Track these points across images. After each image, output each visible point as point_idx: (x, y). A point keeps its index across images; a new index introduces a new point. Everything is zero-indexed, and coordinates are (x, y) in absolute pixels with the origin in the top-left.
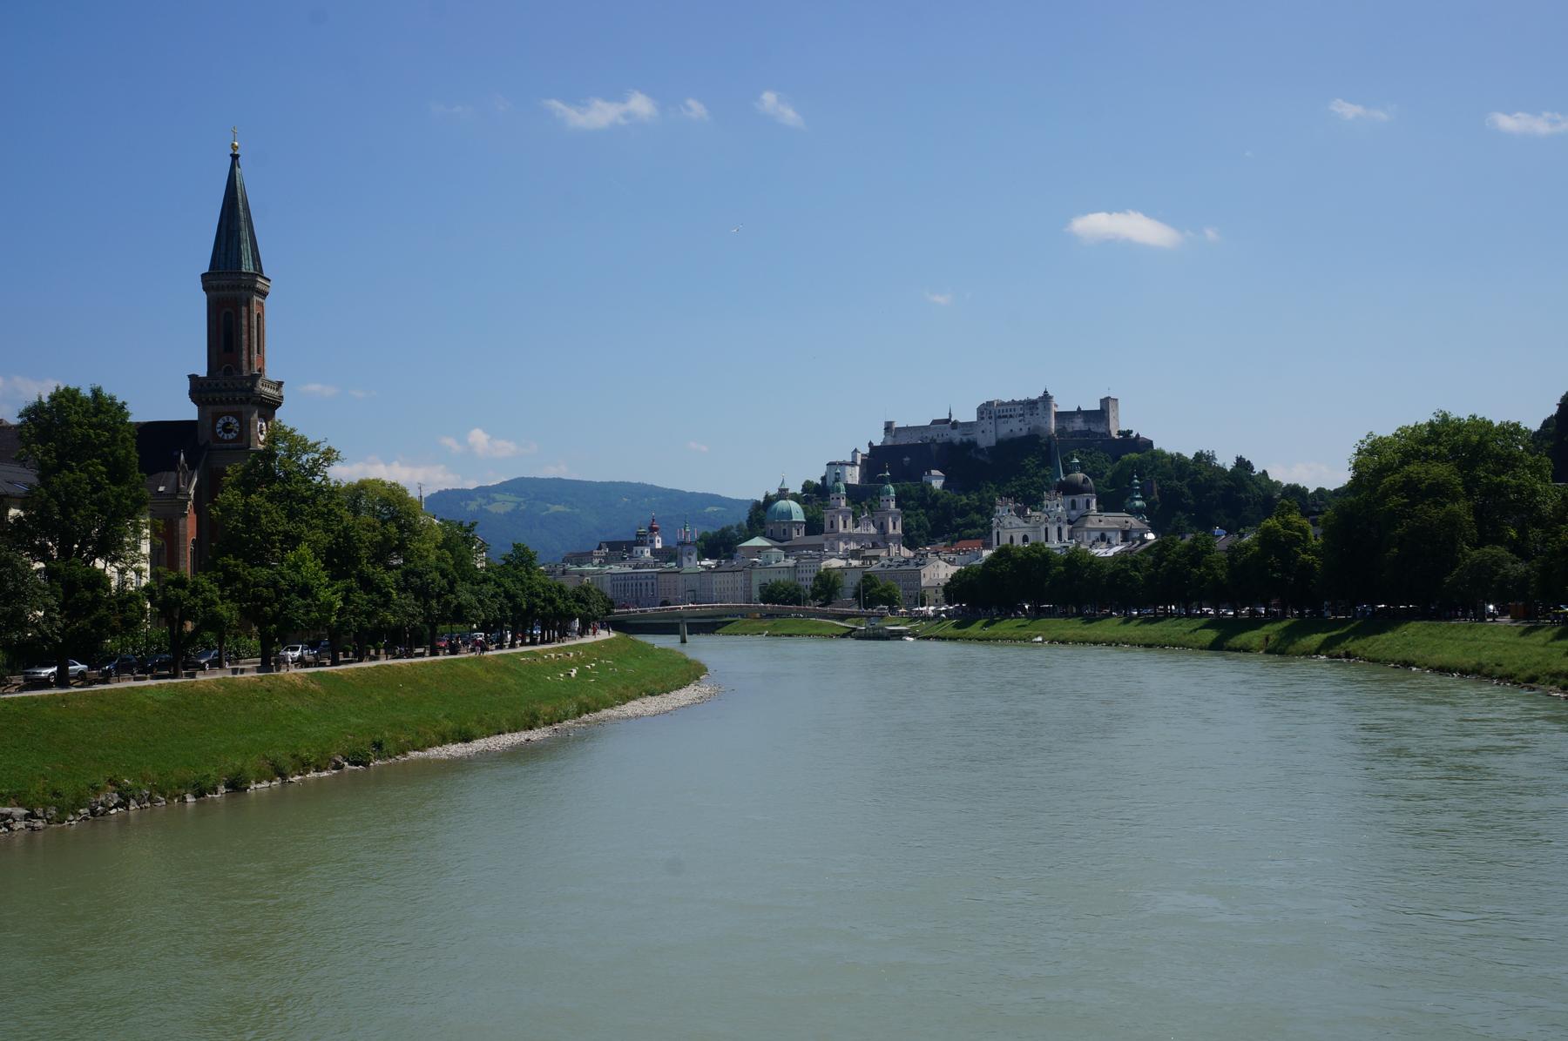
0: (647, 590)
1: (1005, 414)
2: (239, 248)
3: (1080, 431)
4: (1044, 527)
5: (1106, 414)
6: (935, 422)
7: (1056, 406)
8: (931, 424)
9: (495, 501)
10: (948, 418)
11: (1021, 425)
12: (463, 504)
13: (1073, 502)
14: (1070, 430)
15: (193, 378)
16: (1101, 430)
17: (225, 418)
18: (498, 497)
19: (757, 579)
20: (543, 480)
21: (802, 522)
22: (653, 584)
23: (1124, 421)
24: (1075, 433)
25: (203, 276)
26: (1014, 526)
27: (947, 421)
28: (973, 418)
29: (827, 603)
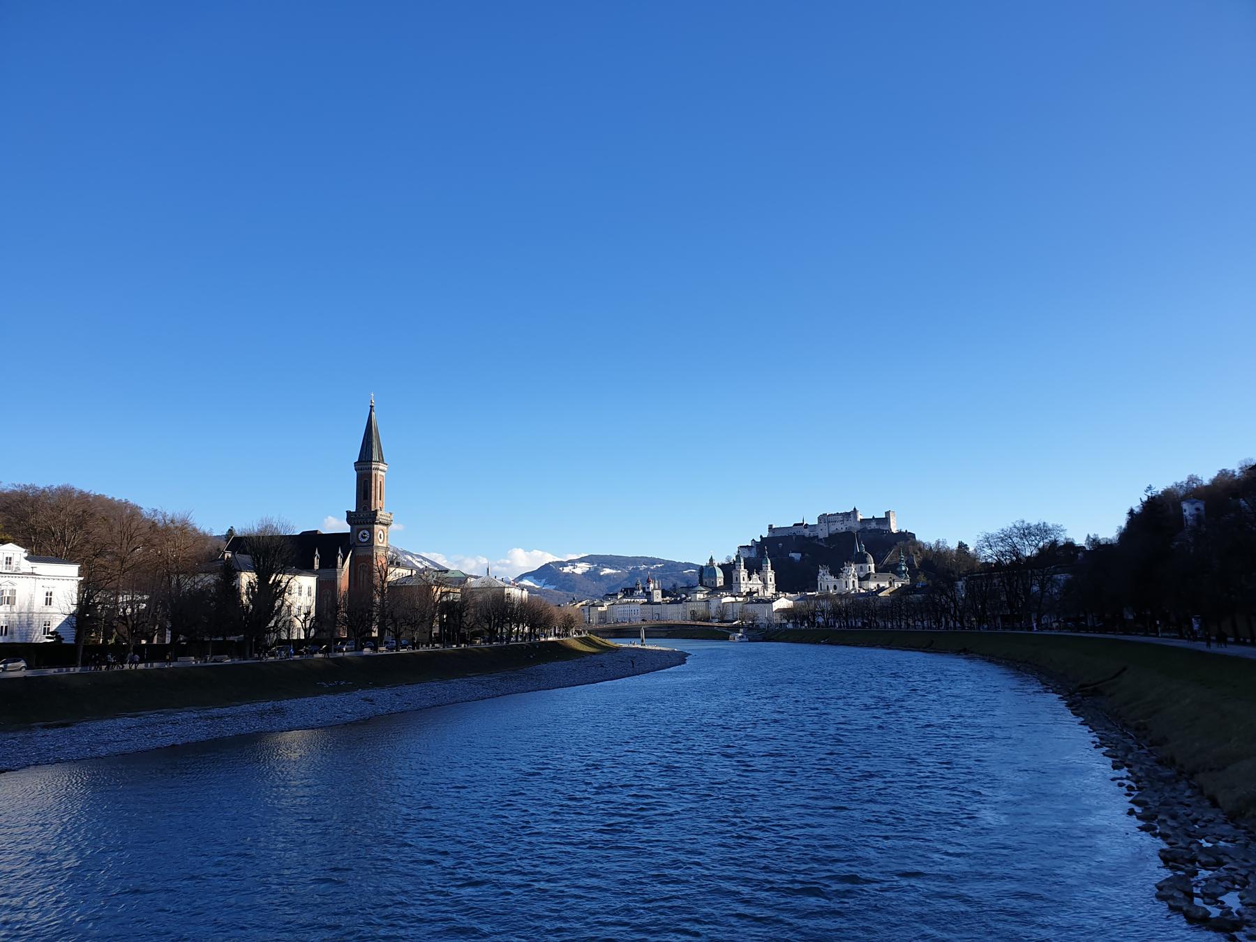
6: (795, 525)
10: (802, 522)
11: (842, 526)
12: (561, 569)
14: (869, 529)
18: (579, 565)
24: (871, 531)
25: (355, 463)
27: (802, 524)
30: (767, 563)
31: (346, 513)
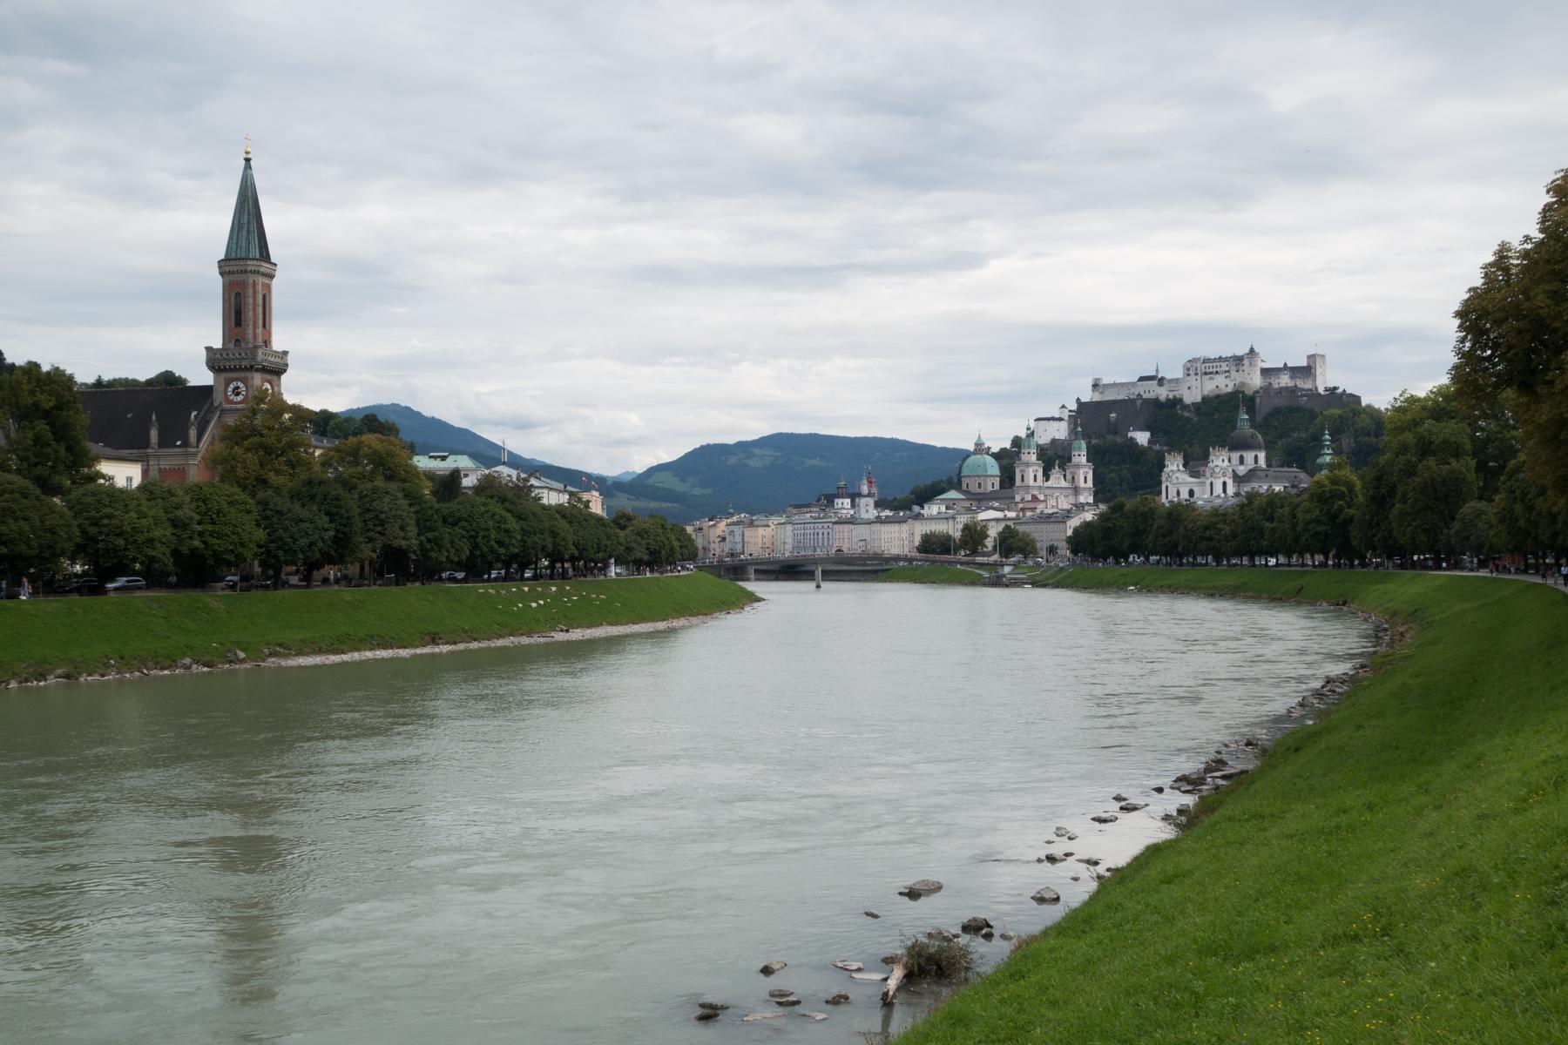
0: (823, 539)
1: (1211, 370)
3: (1287, 388)
4: (1222, 480)
5: (1313, 371)
6: (1142, 379)
9: (753, 455)
10: (1155, 374)
11: (1227, 381)
12: (724, 458)
13: (1242, 458)
14: (1276, 386)
15: (208, 349)
17: (235, 383)
18: (757, 451)
20: (800, 435)
21: (997, 476)
22: (828, 534)
25: (219, 262)
26: (1180, 480)
29: (974, 552)
30: (1080, 449)
31: (204, 351)
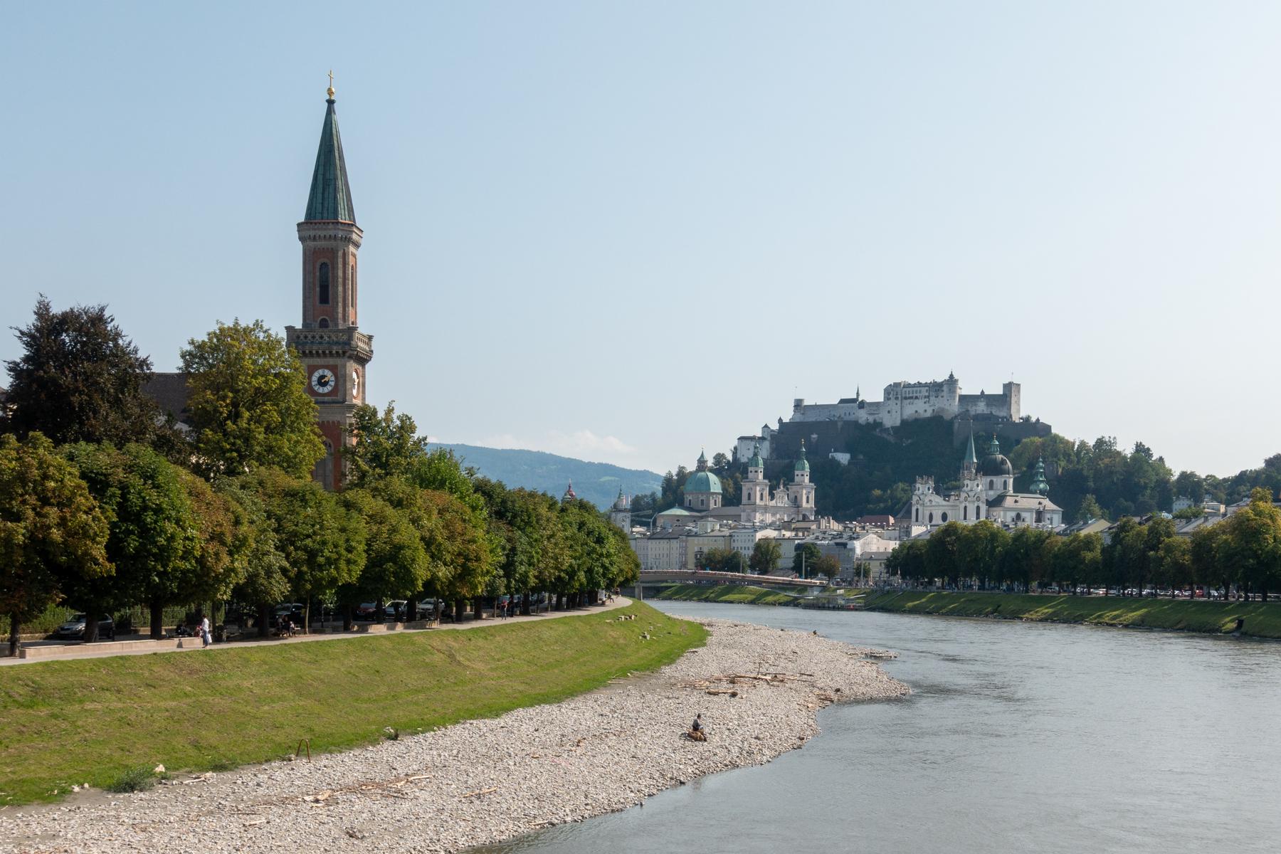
1: (911, 395)
2: (335, 197)
3: (983, 415)
4: (963, 505)
5: (1008, 399)
6: (843, 401)
7: (960, 389)
8: (839, 403)
10: (855, 397)
13: (991, 483)
14: (973, 413)
16: (1002, 414)
19: (695, 545)
23: (1026, 408)
24: (977, 418)
25: (299, 225)
26: (934, 504)
27: (853, 401)
28: (880, 398)
30: (803, 469)
